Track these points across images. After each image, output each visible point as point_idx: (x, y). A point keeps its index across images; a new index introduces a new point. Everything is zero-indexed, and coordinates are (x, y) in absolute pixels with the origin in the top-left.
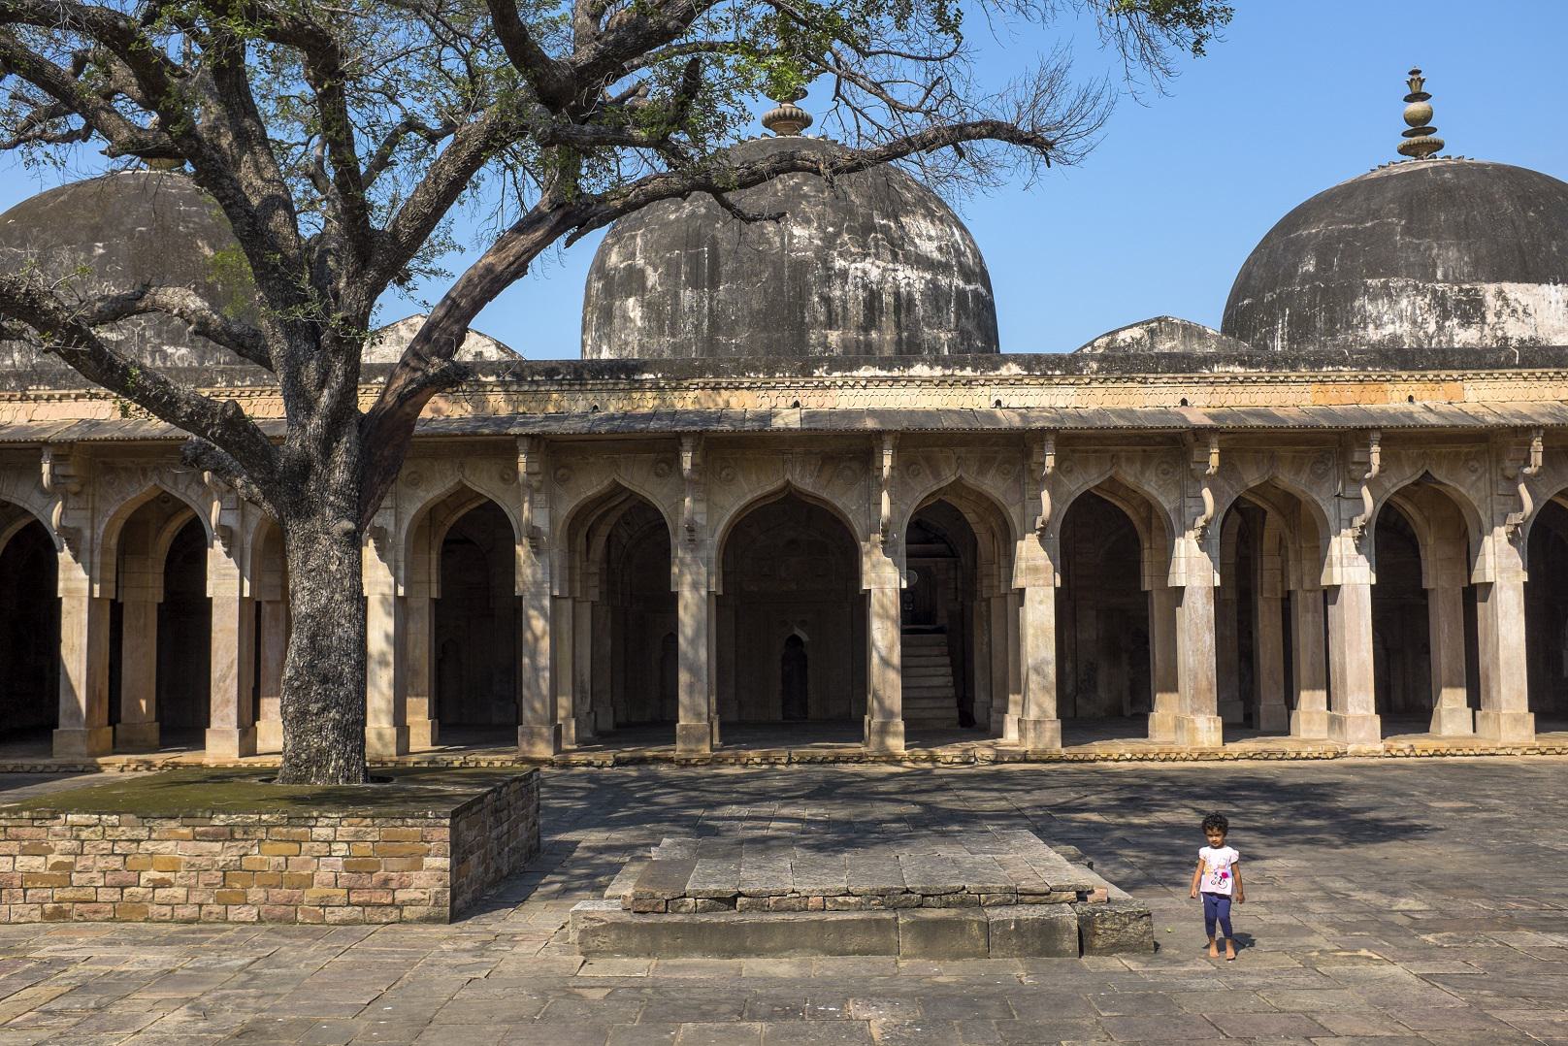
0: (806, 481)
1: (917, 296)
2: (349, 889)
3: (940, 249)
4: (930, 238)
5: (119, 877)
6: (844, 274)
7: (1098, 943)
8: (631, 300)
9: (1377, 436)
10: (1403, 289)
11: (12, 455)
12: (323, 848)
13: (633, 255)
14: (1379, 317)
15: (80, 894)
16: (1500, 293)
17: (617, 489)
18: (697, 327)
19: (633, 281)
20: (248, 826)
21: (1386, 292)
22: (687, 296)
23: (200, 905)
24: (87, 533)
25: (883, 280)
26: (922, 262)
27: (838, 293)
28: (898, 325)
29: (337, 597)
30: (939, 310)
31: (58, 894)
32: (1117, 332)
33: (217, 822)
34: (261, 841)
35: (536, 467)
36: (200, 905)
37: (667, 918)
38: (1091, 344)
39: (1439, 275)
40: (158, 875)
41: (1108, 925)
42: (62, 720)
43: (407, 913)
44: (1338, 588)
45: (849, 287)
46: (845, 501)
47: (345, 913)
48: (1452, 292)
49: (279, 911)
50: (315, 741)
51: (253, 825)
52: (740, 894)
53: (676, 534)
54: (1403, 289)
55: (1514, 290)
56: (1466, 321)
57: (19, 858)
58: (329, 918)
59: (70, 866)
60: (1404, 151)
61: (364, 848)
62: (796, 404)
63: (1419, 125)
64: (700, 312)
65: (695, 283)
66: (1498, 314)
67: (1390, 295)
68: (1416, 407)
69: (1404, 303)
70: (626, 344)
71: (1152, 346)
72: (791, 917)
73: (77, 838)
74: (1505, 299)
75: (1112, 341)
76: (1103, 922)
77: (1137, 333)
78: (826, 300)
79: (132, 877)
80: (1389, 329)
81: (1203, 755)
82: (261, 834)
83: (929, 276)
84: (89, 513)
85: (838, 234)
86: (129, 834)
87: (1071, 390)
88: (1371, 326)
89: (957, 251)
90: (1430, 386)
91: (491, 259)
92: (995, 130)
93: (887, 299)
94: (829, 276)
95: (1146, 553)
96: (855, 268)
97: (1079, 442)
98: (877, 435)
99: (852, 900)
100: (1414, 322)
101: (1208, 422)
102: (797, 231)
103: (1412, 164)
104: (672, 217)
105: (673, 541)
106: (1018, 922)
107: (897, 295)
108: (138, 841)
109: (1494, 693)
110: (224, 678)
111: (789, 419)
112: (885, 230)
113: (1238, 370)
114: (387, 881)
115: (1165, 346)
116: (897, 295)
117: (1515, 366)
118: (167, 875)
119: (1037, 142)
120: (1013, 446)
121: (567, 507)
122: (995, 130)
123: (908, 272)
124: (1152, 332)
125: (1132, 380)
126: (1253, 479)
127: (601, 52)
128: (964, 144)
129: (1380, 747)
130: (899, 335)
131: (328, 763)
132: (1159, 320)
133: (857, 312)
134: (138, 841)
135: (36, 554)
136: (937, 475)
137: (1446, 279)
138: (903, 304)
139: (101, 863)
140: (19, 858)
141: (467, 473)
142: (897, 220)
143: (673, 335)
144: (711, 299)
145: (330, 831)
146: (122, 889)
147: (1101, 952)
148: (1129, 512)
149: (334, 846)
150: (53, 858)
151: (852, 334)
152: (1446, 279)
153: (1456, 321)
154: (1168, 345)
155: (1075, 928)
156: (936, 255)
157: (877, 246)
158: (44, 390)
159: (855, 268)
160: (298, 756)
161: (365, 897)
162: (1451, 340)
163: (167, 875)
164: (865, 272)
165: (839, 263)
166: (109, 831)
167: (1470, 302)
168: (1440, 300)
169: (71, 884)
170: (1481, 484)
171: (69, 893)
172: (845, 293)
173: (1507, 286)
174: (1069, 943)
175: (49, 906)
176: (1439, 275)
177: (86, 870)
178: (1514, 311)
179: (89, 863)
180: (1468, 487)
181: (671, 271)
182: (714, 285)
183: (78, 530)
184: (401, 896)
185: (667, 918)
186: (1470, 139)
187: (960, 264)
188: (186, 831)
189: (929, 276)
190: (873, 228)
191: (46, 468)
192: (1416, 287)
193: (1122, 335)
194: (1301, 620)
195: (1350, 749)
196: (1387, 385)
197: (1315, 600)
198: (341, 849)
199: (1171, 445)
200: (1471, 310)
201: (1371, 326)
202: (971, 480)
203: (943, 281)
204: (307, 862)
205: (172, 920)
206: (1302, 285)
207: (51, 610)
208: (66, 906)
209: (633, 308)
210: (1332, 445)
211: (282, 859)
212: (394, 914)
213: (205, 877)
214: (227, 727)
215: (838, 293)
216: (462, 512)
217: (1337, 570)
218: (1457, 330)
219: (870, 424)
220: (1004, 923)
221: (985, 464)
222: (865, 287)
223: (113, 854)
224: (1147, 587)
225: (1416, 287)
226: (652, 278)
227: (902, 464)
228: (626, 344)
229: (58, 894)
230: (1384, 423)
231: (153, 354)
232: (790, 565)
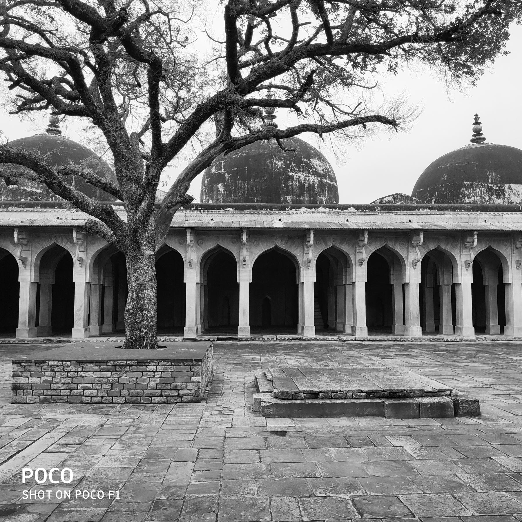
0: (283, 246)
1: (316, 185)
2: (162, 390)
3: (323, 170)
4: (320, 166)
5: (71, 386)
6: (292, 177)
7: (460, 412)
8: (220, 185)
9: (476, 233)
10: (477, 185)
11: (4, 231)
12: (152, 374)
13: (221, 170)
14: (469, 195)
15: (54, 393)
16: (510, 187)
17: (218, 246)
18: (243, 194)
19: (220, 178)
20: (122, 366)
21: (471, 186)
22: (239, 183)
23: (102, 397)
24: (29, 259)
25: (305, 179)
26: (316, 173)
27: (291, 184)
28: (310, 195)
29: (147, 279)
30: (322, 190)
31: (45, 392)
32: (383, 198)
33: (109, 364)
34: (126, 371)
35: (192, 239)
36: (102, 397)
37: (294, 402)
38: (374, 202)
39: (490, 181)
40: (85, 385)
41: (464, 405)
42: (19, 325)
43: (184, 399)
44: (460, 284)
45: (294, 182)
46: (297, 253)
47: (160, 399)
48: (494, 187)
49: (133, 399)
50: (138, 333)
51: (124, 365)
52: (321, 392)
53: (239, 262)
54: (477, 185)
55: (513, 186)
56: (499, 197)
57: (30, 378)
58: (154, 401)
59: (50, 383)
60: (472, 141)
61: (167, 374)
62: (280, 220)
63: (477, 132)
64: (244, 189)
65: (243, 180)
66: (509, 194)
67: (473, 187)
68: (487, 224)
69: (478, 190)
70: (218, 199)
71: (395, 203)
72: (342, 401)
73: (53, 371)
74: (511, 189)
75: (382, 201)
76: (462, 404)
77: (390, 198)
78: (287, 186)
79: (75, 386)
80: (473, 199)
81: (416, 340)
82: (127, 369)
83: (319, 179)
84: (30, 252)
85: (290, 164)
86: (74, 369)
87: (372, 216)
88: (466, 198)
89: (328, 170)
90: (492, 217)
91: (200, 159)
92: (378, 118)
93: (306, 186)
94: (289, 178)
95: (392, 271)
96: (296, 175)
97: (376, 234)
98: (309, 230)
99: (363, 394)
100: (481, 197)
101: (420, 228)
102: (277, 162)
103: (476, 145)
104: (234, 157)
105: (238, 265)
106: (431, 404)
107: (309, 184)
108: (78, 372)
109: (511, 320)
110: (79, 310)
111: (279, 225)
112: (306, 163)
113: (428, 211)
114: (176, 386)
115: (399, 203)
116: (309, 184)
117: (520, 211)
118: (89, 385)
119: (393, 123)
120: (354, 235)
121: (202, 252)
122: (378, 118)
123: (313, 177)
124: (395, 198)
125: (392, 213)
126: (432, 247)
127: (257, 76)
128: (366, 124)
129: (474, 338)
130: (310, 198)
131: (144, 341)
132: (397, 194)
133: (297, 190)
134: (78, 372)
135: (11, 267)
136: (326, 244)
137: (492, 183)
138: (312, 187)
139: (63, 380)
140: (30, 378)
141: (167, 240)
142: (309, 160)
143: (235, 197)
144: (248, 185)
145: (154, 367)
146: (71, 390)
147: (461, 416)
148: (386, 258)
149: (156, 373)
150: (43, 379)
151: (295, 198)
152: (492, 183)
153: (495, 196)
154: (400, 203)
155: (452, 406)
156: (322, 172)
157: (303, 168)
158: (15, 209)
159: (296, 175)
160: (131, 338)
161: (167, 393)
162: (494, 203)
163: (89, 385)
164: (299, 177)
165: (291, 174)
166: (66, 368)
167: (500, 190)
168: (490, 190)
169: (51, 389)
170: (508, 250)
171: (50, 392)
172: (293, 184)
173: (512, 185)
174: (451, 412)
175: (42, 397)
176: (490, 181)
177: (57, 383)
178: (515, 193)
179: (58, 380)
180: (505, 251)
181: (234, 175)
182: (249, 180)
183: (26, 258)
184: (182, 392)
185: (294, 402)
186: (493, 137)
187: (329, 174)
188: (97, 368)
189: (319, 179)
190: (302, 162)
191: (16, 236)
192: (482, 185)
193: (385, 199)
194: (444, 294)
195: (465, 338)
196: (478, 217)
197: (448, 288)
198: (158, 374)
199: (406, 235)
200: (500, 193)
201: (466, 198)
202: (338, 245)
203: (324, 181)
204: (145, 380)
205: (91, 403)
206: (442, 184)
207: (16, 286)
208: (49, 397)
209: (221, 187)
210: (460, 236)
211: (135, 379)
212: (179, 400)
213: (104, 386)
214: (80, 328)
215: (291, 184)
216: (163, 254)
217: (460, 278)
218: (495, 199)
219: (306, 226)
220: (426, 404)
221: (342, 240)
222: (299, 182)
223: (67, 377)
224: (392, 283)
225: (482, 185)
226: (227, 177)
227: (316, 240)
228: (218, 199)
229: (45, 392)
230: (479, 229)
231: (52, 198)
232: (276, 273)
